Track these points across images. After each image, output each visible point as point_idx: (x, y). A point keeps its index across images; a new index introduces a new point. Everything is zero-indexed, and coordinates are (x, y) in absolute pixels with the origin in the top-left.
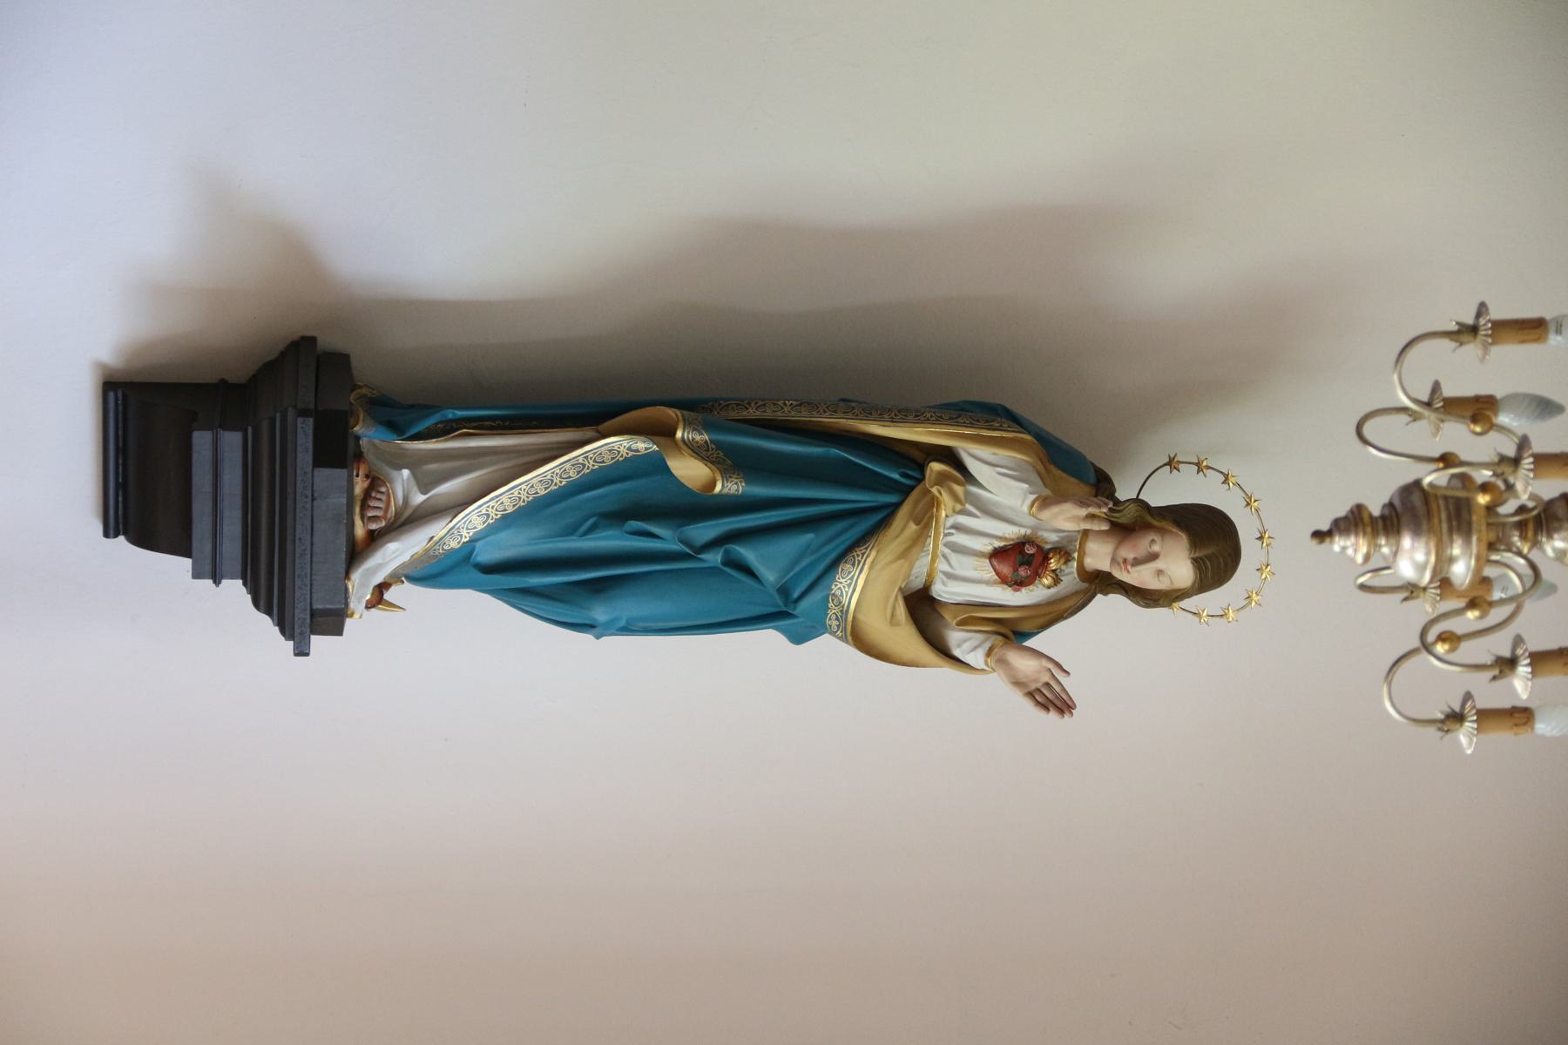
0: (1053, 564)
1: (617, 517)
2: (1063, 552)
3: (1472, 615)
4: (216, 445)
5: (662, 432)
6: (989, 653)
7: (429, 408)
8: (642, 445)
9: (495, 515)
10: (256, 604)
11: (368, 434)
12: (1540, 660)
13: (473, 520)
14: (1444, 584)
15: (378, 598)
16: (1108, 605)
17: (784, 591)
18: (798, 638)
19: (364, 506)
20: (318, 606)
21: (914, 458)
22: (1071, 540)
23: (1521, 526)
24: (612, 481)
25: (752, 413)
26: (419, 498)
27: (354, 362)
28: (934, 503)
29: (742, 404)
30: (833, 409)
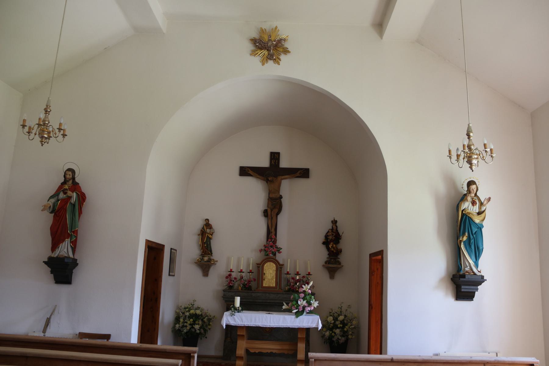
0: (474, 200)
1: (470, 246)
2: (473, 199)
3: (481, 155)
4: (463, 289)
5: (461, 241)
6: (484, 206)
7: (458, 266)
8: (462, 243)
9: (470, 259)
10: (481, 285)
11: (462, 273)
12: (485, 148)
13: (471, 262)
14: (477, 158)
15: (480, 272)
16: (478, 194)
17: (478, 228)
18: (483, 227)
19: (470, 273)
20: (481, 278)
21: (463, 214)
22: (471, 198)
23: (471, 151)
24: (466, 246)
25: (458, 232)
26: (469, 267)
27: (454, 274)
28: (468, 212)
29: (457, 233)
30: (458, 223)
